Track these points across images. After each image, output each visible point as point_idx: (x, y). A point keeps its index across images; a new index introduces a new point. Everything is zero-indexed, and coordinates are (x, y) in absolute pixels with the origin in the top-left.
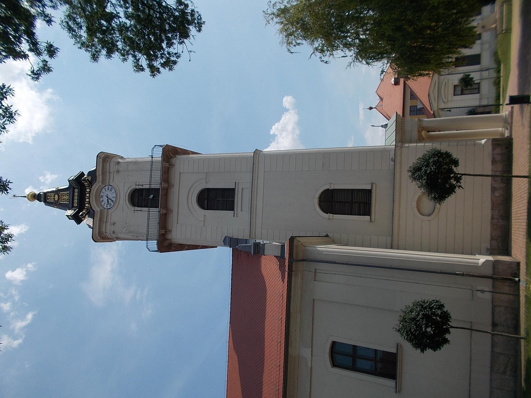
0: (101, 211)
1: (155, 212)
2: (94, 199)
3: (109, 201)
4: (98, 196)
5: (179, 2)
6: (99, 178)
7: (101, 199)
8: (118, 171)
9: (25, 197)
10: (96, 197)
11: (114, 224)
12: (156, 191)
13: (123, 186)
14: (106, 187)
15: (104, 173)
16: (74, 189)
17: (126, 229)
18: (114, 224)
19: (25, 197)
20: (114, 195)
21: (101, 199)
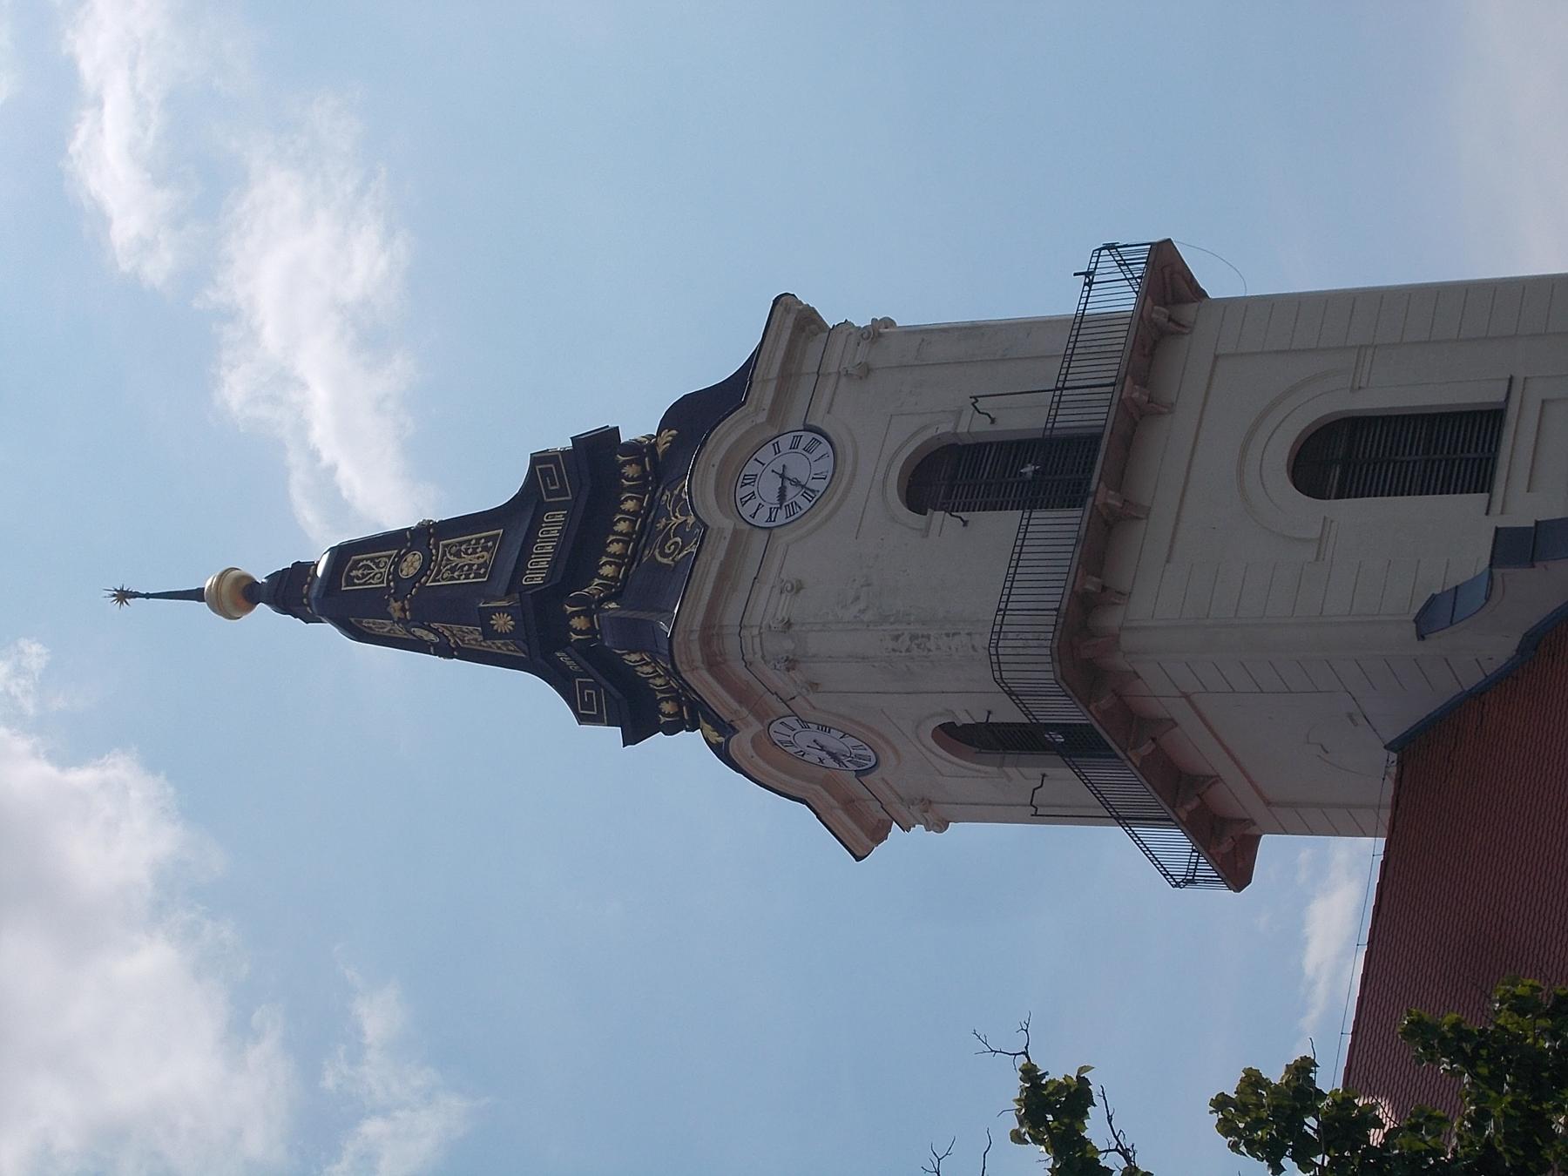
0: (736, 533)
1: (1058, 526)
2: (712, 482)
3: (791, 492)
4: (734, 477)
5: (1277, 1169)
6: (763, 394)
7: (743, 492)
8: (866, 371)
9: (197, 595)
10: (720, 473)
11: (798, 588)
12: (1086, 444)
13: (880, 436)
14: (786, 442)
15: (788, 377)
16: (541, 509)
17: (862, 606)
18: (798, 588)
19: (197, 595)
20: (826, 466)
21: (743, 492)
